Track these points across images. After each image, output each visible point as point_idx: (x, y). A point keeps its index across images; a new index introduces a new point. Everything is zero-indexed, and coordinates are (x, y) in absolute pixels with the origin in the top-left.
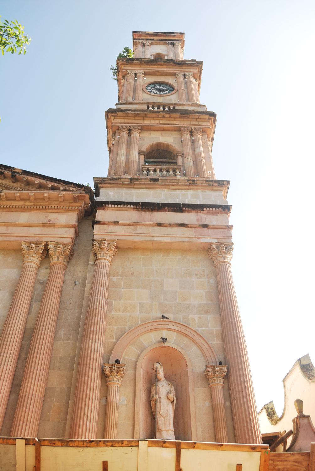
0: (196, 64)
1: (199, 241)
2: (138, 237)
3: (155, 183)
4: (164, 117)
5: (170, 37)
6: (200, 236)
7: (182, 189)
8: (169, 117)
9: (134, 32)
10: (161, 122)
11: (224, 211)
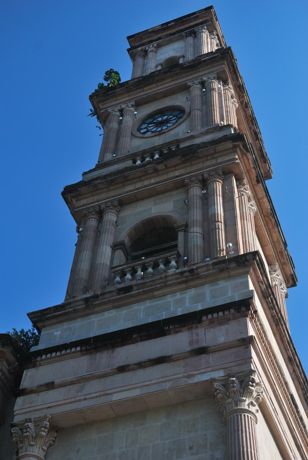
0: (220, 56)
1: (190, 381)
2: (86, 401)
3: (127, 294)
4: (156, 171)
5: (191, 22)
6: (191, 373)
7: (175, 292)
8: (164, 167)
9: (128, 38)
10: (153, 181)
11: (239, 312)
